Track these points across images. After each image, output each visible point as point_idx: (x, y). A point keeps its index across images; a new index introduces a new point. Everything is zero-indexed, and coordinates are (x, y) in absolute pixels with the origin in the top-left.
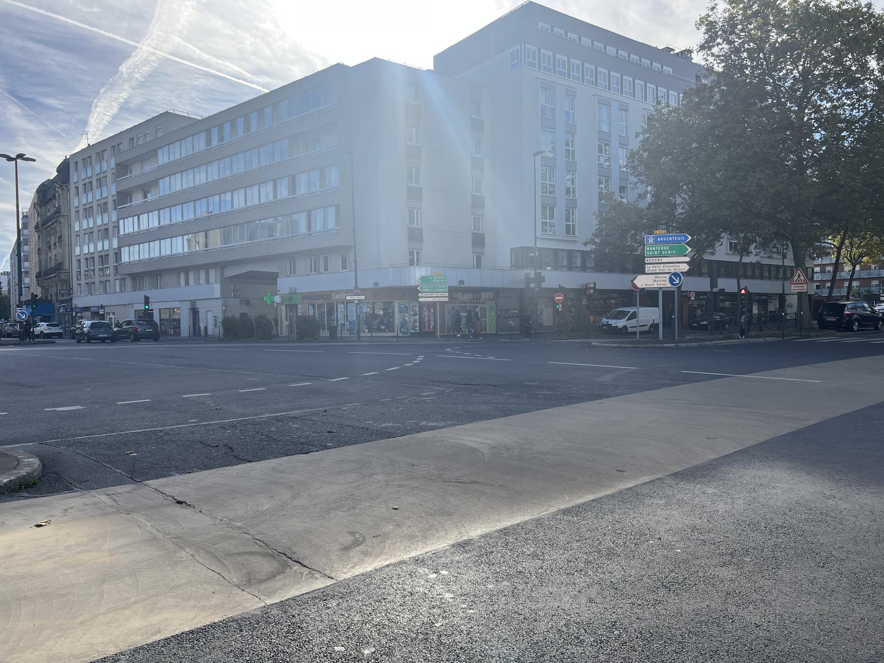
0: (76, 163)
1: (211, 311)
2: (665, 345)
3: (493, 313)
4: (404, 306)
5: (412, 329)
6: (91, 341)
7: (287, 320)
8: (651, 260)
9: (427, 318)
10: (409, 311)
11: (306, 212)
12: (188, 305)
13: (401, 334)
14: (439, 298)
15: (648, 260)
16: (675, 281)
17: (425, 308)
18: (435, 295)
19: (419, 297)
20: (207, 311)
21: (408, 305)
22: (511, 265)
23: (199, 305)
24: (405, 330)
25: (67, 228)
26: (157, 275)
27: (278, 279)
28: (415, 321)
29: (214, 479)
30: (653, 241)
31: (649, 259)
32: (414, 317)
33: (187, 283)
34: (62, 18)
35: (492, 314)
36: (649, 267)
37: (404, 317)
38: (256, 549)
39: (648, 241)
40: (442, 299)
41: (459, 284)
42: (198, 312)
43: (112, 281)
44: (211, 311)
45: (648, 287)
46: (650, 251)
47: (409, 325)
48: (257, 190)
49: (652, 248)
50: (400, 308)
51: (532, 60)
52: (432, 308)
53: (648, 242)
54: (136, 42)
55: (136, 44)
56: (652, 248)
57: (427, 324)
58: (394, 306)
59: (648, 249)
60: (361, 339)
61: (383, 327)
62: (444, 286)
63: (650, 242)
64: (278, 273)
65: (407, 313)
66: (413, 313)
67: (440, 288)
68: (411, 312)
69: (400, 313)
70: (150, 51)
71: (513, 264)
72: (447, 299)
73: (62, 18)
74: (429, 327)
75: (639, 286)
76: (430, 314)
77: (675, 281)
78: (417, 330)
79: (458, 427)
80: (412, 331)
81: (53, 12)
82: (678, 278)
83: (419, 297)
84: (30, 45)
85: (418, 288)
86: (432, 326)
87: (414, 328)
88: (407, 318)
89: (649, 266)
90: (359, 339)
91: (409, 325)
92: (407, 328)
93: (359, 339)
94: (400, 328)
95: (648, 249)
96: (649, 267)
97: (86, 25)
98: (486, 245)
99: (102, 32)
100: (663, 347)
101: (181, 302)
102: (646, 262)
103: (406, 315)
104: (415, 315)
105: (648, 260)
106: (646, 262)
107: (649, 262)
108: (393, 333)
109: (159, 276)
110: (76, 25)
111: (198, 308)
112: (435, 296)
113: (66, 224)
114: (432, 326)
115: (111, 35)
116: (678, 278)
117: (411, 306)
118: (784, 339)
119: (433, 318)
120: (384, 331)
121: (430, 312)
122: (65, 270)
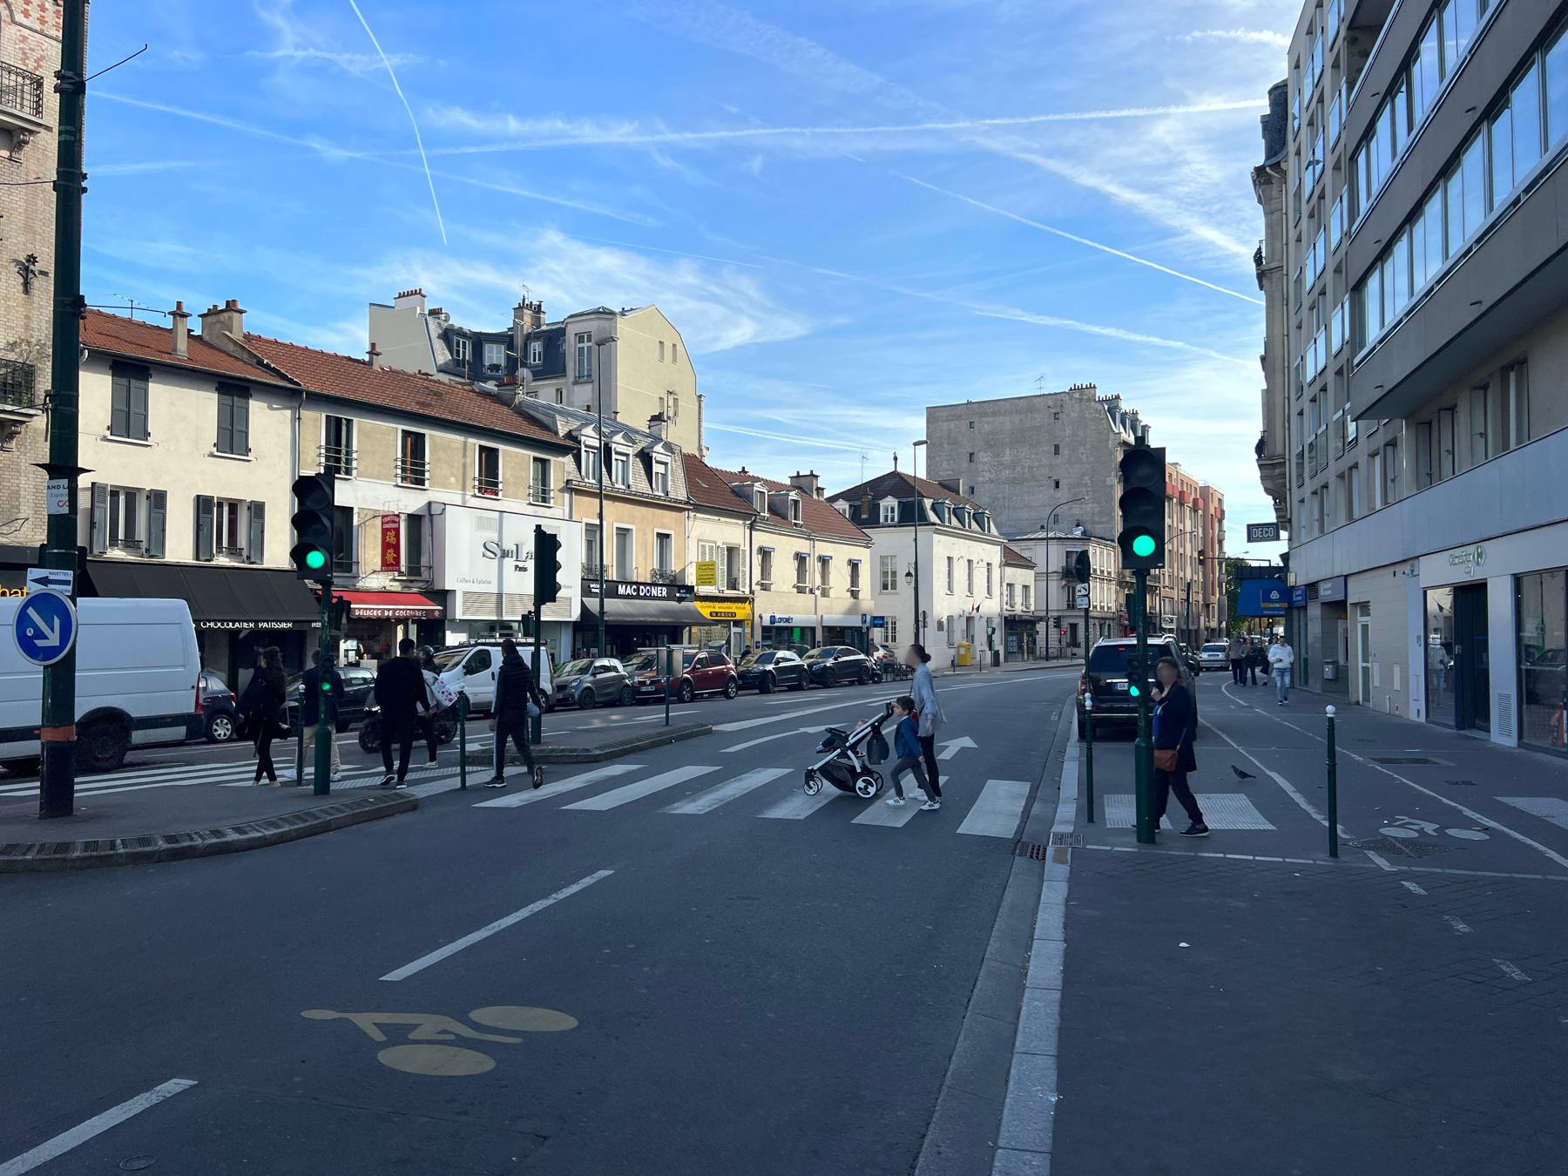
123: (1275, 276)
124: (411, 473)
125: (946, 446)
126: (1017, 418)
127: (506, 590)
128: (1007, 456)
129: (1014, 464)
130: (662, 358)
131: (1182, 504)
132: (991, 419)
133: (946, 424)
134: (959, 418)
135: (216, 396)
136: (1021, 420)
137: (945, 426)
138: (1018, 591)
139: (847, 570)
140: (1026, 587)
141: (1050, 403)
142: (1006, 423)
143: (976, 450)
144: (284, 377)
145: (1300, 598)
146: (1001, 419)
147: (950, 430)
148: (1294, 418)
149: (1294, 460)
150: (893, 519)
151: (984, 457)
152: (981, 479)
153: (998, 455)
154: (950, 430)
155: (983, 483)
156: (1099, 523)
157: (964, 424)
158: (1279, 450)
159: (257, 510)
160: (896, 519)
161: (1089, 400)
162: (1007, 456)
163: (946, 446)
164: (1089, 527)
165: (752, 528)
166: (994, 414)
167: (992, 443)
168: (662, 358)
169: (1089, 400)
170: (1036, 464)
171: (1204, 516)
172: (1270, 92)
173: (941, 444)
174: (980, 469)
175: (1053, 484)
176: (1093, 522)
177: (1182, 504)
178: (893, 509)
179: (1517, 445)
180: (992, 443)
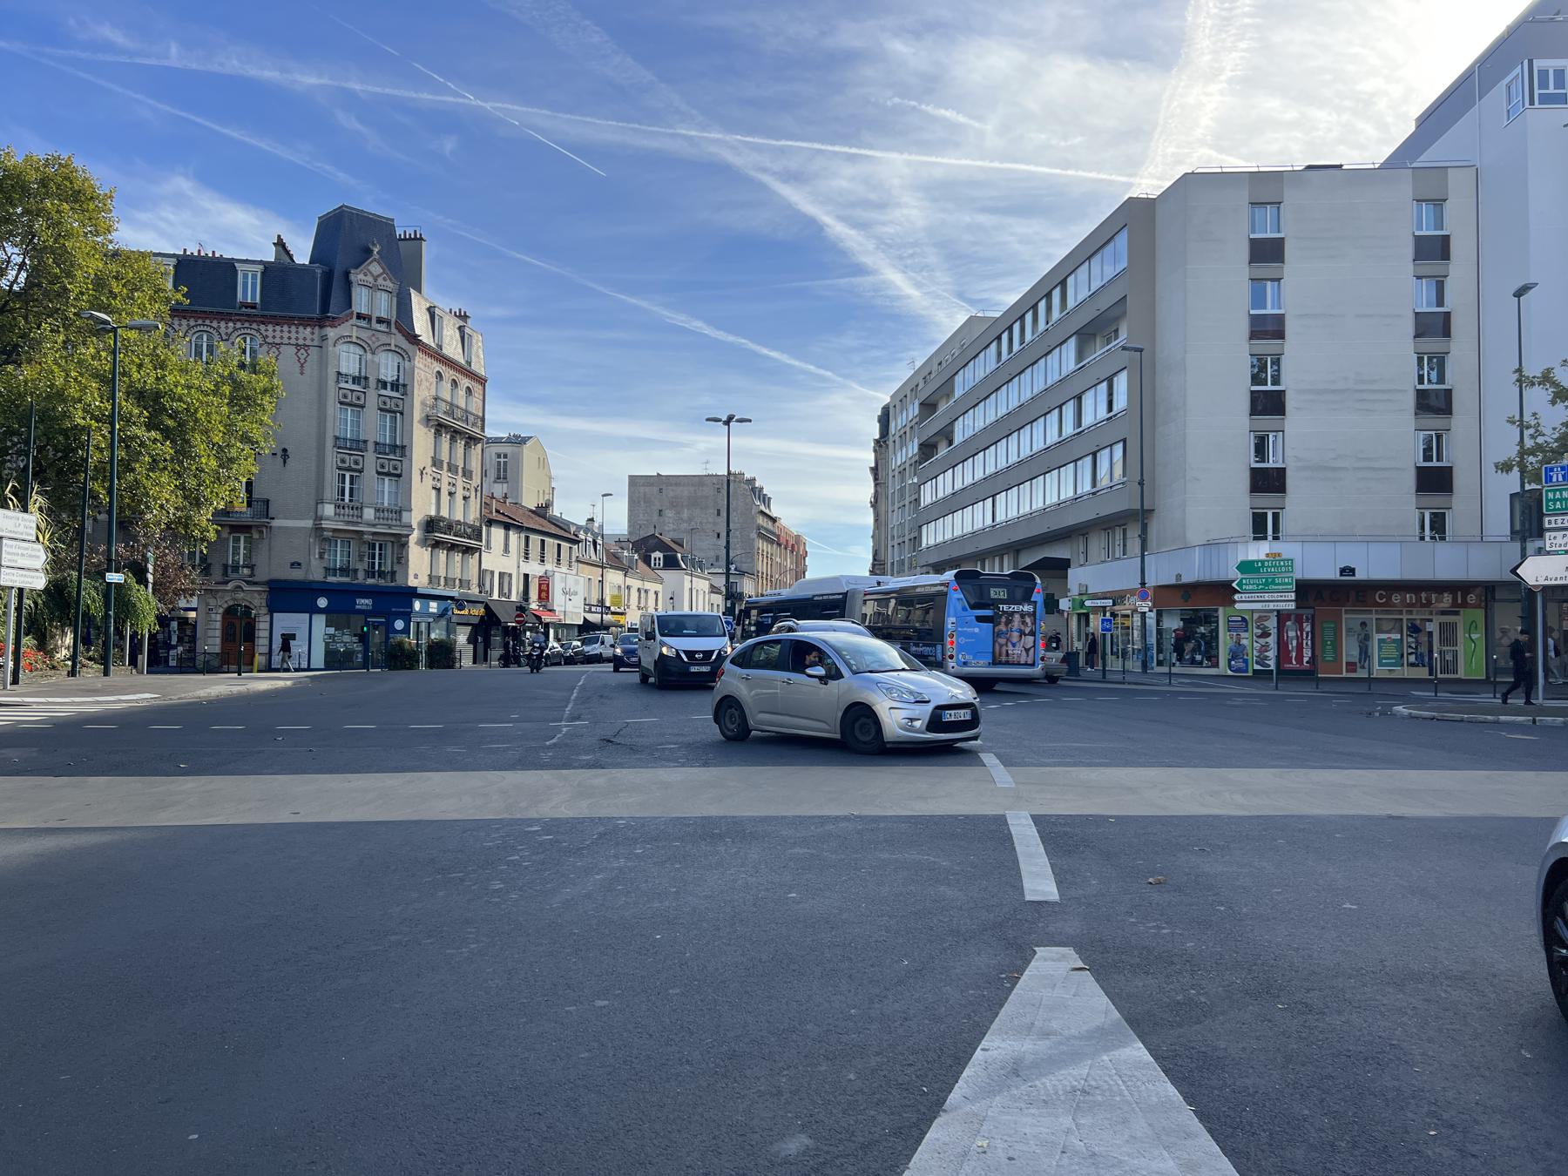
0: (895, 406)
2: (1503, 718)
3: (1478, 635)
4: (1240, 619)
5: (1257, 663)
6: (621, 669)
7: (1079, 640)
8: (1559, 522)
9: (1294, 643)
10: (1250, 626)
13: (1230, 673)
14: (1276, 604)
15: (1550, 522)
17: (1288, 623)
18: (1267, 597)
19: (1235, 602)
21: (1247, 617)
22: (1513, 532)
24: (1242, 665)
25: (884, 500)
27: (1069, 571)
28: (1265, 648)
30: (1563, 476)
31: (1553, 519)
32: (1262, 641)
34: (1023, 167)
35: (1474, 636)
36: (1555, 538)
37: (1239, 639)
39: (1551, 477)
40: (1281, 606)
41: (1341, 575)
45: (1553, 582)
46: (1554, 501)
47: (1250, 655)
48: (1029, 430)
49: (1561, 495)
50: (1229, 621)
52: (1307, 620)
53: (1551, 481)
54: (1131, 175)
55: (1132, 180)
56: (1561, 495)
57: (1294, 654)
58: (1217, 617)
59: (1551, 495)
60: (1109, 676)
61: (1198, 657)
62: (1286, 580)
63: (1554, 479)
64: (1069, 560)
65: (1247, 631)
66: (1260, 631)
67: (1278, 584)
68: (1255, 631)
69: (1229, 631)
70: (1152, 185)
71: (1518, 527)
72: (1292, 606)
73: (1023, 167)
74: (1300, 658)
75: (1531, 581)
76: (1302, 634)
78: (1269, 666)
79: (684, 816)
80: (1257, 667)
81: (1016, 161)
83: (1235, 602)
84: (982, 218)
85: (1234, 585)
86: (1306, 659)
87: (1262, 660)
88: (1244, 642)
89: (1553, 534)
90: (1104, 677)
91: (1250, 655)
92: (1246, 661)
93: (1104, 677)
94: (1229, 661)
95: (1551, 495)
96: (1555, 538)
97: (1056, 168)
98: (1454, 491)
99: (1081, 173)
100: (1497, 722)
102: (1547, 526)
103: (1243, 635)
104: (1265, 634)
105: (1550, 522)
106: (1547, 526)
107: (1553, 525)
108: (1216, 669)
112: (1267, 599)
113: (883, 493)
114: (1306, 659)
117: (1254, 618)
119: (1309, 643)
120: (1200, 664)
121: (1302, 630)
122: (881, 561)
123: (882, 485)
124: (1123, 650)
125: (642, 503)
126: (692, 489)
127: (567, 610)
128: (685, 515)
129: (690, 520)
130: (539, 467)
131: (786, 548)
132: (674, 488)
133: (642, 488)
134: (652, 485)
135: (503, 531)
136: (695, 491)
137: (642, 489)
138: (715, 606)
139: (654, 596)
140: (718, 605)
141: (715, 481)
142: (685, 492)
143: (664, 508)
144: (515, 520)
145: (1350, 650)
146: (681, 488)
147: (645, 492)
148: (890, 548)
149: (889, 564)
150: (659, 564)
151: (669, 514)
152: (667, 528)
153: (679, 513)
154: (645, 492)
155: (669, 531)
156: (745, 563)
157: (655, 489)
158: (883, 558)
159: (510, 575)
160: (662, 565)
161: (740, 482)
162: (685, 515)
163: (642, 503)
164: (739, 565)
165: (625, 576)
166: (676, 484)
167: (675, 504)
168: (539, 467)
169: (740, 482)
170: (705, 521)
171: (797, 555)
172: (882, 409)
173: (639, 502)
174: (667, 521)
175: (716, 536)
176: (742, 562)
177: (786, 548)
178: (659, 559)
179: (1077, 364)
180: (675, 504)
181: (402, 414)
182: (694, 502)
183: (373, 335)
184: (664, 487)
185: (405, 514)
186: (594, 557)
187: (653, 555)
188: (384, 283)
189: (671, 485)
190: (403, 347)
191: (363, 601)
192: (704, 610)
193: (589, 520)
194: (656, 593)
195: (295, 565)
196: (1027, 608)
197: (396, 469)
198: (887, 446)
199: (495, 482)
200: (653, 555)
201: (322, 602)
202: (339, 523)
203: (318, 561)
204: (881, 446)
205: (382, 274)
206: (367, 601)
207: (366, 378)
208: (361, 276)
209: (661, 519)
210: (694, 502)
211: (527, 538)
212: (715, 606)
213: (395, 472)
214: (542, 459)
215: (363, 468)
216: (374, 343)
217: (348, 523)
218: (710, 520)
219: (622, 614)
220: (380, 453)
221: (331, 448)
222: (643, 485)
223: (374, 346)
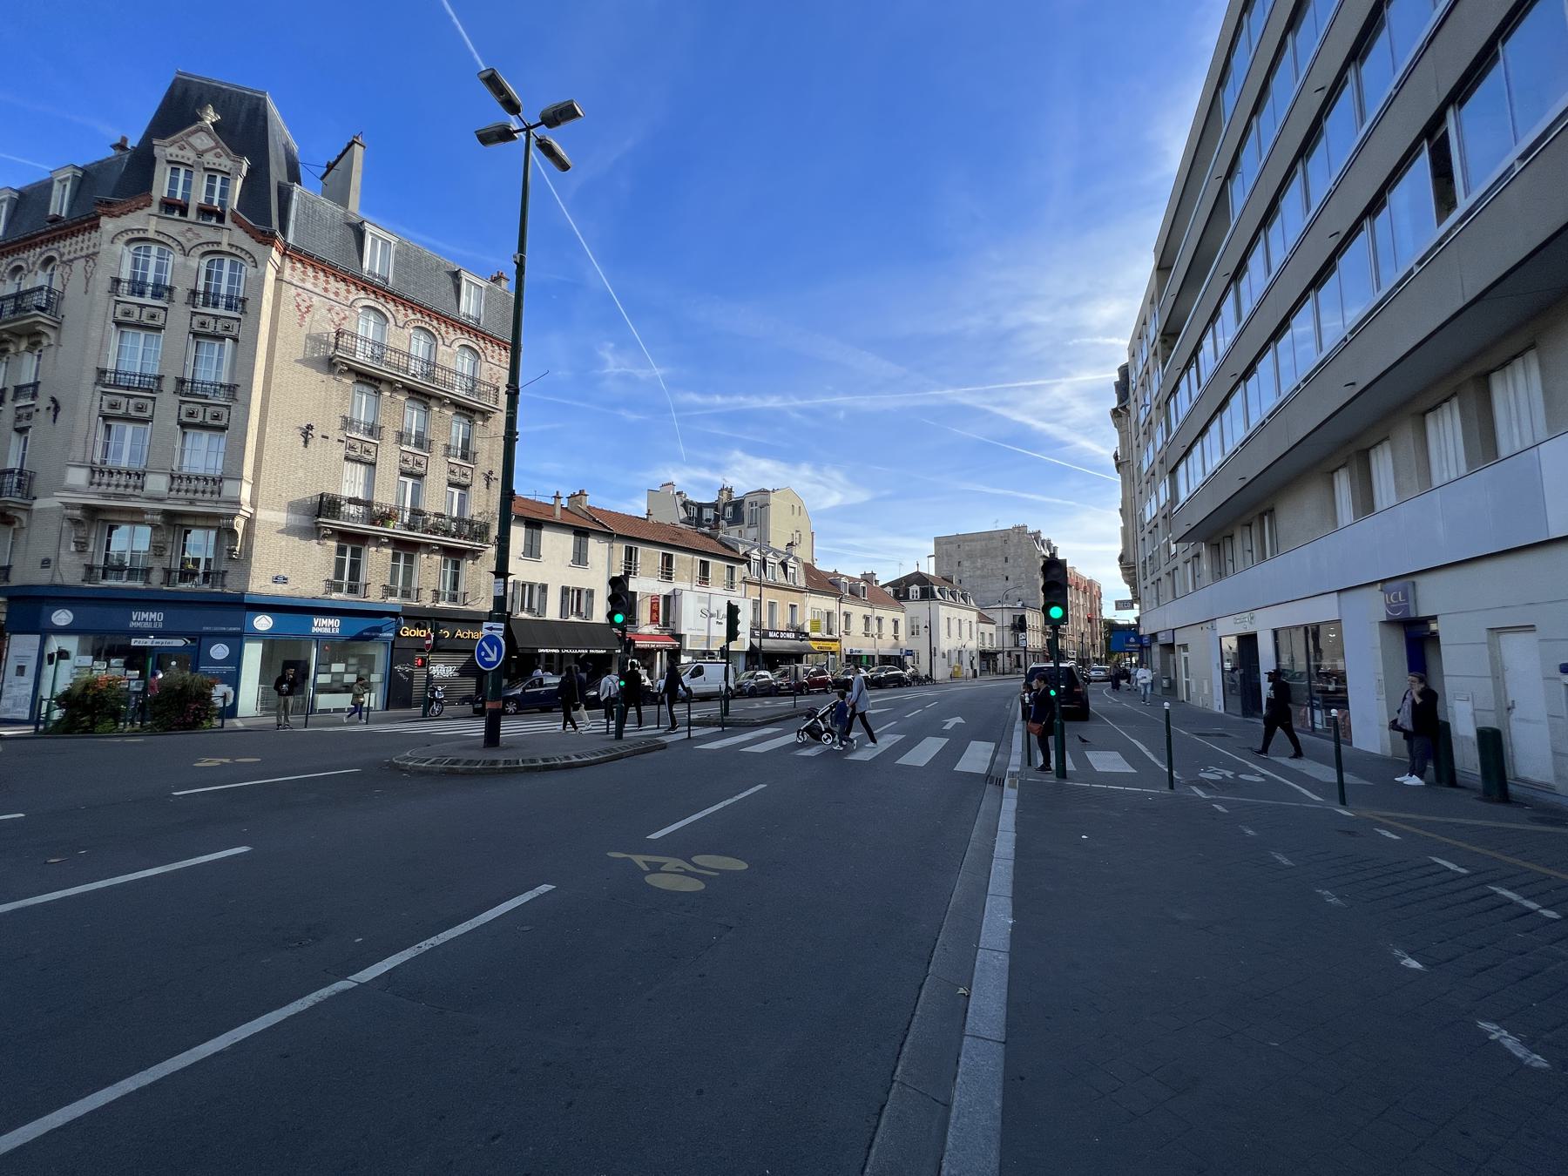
1: (1530, 628)
11: (502, 594)
12: (1375, 606)
16: (489, 656)
20: (1496, 631)
23: (1430, 599)
26: (1262, 515)
29: (375, 678)
33: (1365, 503)
38: (1193, 371)
42: (1435, 637)
43: (1181, 565)
44: (1530, 628)
51: (672, 555)
77: (489, 656)
82: (495, 648)
101: (1343, 595)
109: (1266, 518)
110: (148, 670)
111: (1434, 618)
115: (1052, 460)
116: (495, 648)
118: (492, 737)
123: (1126, 465)
126: (983, 543)
129: (983, 566)
130: (793, 513)
134: (951, 543)
135: (573, 537)
137: (944, 547)
138: (987, 636)
142: (978, 545)
144: (605, 527)
148: (1140, 542)
151: (966, 564)
152: (965, 576)
157: (956, 545)
159: (591, 593)
165: (840, 601)
167: (971, 556)
168: (793, 513)
180: (971, 556)
181: (235, 340)
182: (986, 553)
183: (190, 230)
184: (961, 543)
185: (227, 485)
186: (782, 580)
187: (911, 588)
188: (216, 160)
189: (967, 541)
190: (245, 247)
191: (145, 615)
192: (501, 630)
193: (788, 545)
194: (896, 622)
195: (46, 563)
196: (373, 699)
197: (216, 417)
198: (1128, 412)
199: (748, 527)
200: (911, 588)
201: (62, 617)
202: (180, 502)
203: (76, 557)
204: (1120, 415)
205: (212, 149)
206: (153, 616)
207: (171, 289)
208: (174, 150)
209: (960, 568)
210: (986, 553)
211: (705, 565)
212: (987, 636)
213: (216, 423)
214: (796, 507)
215: (152, 416)
216: (189, 240)
217: (106, 496)
218: (1000, 566)
219: (835, 640)
220: (187, 395)
221: (91, 388)
222: (946, 544)
223: (188, 246)
